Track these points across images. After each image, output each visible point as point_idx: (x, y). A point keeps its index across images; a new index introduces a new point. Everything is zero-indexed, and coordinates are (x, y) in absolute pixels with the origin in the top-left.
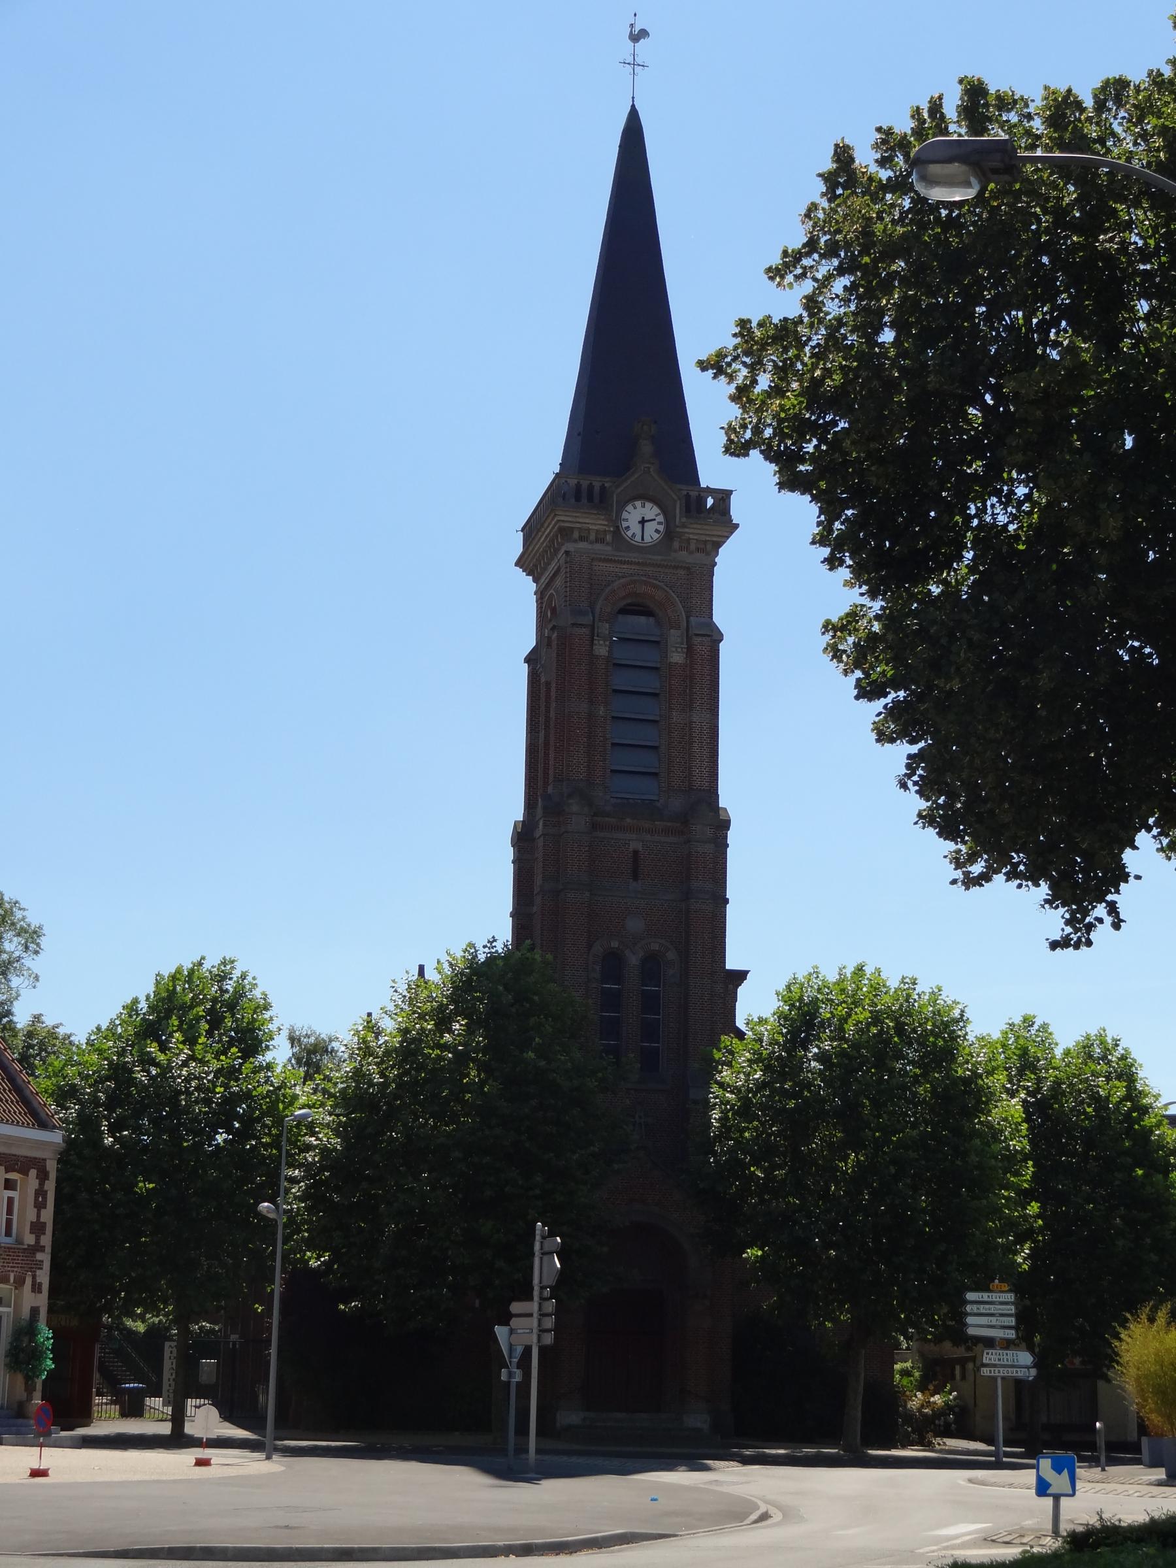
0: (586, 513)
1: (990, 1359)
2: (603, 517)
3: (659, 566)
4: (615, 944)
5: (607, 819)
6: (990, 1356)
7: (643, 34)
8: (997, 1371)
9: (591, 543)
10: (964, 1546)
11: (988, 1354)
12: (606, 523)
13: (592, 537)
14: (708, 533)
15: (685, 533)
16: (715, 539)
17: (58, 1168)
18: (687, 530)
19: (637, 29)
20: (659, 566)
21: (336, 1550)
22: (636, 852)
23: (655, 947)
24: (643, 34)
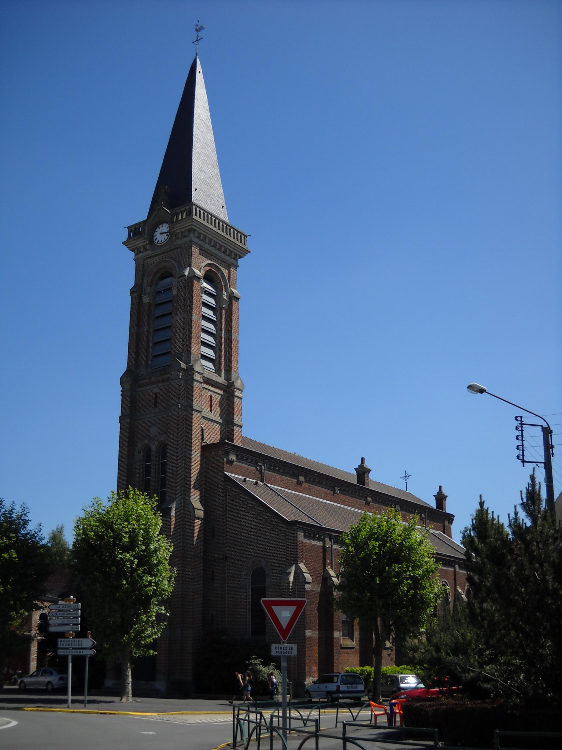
0: (135, 240)
1: (63, 645)
2: (142, 239)
3: (170, 251)
4: (146, 442)
5: (145, 381)
6: (62, 643)
7: (202, 28)
8: (68, 652)
9: (143, 252)
10: (363, 729)
11: (61, 641)
12: (144, 241)
13: (142, 249)
14: (184, 226)
15: (176, 230)
16: (187, 228)
17: (35, 611)
18: (175, 229)
19: (199, 26)
20: (170, 251)
21: (316, 743)
22: (156, 394)
23: (162, 439)
24: (202, 28)
